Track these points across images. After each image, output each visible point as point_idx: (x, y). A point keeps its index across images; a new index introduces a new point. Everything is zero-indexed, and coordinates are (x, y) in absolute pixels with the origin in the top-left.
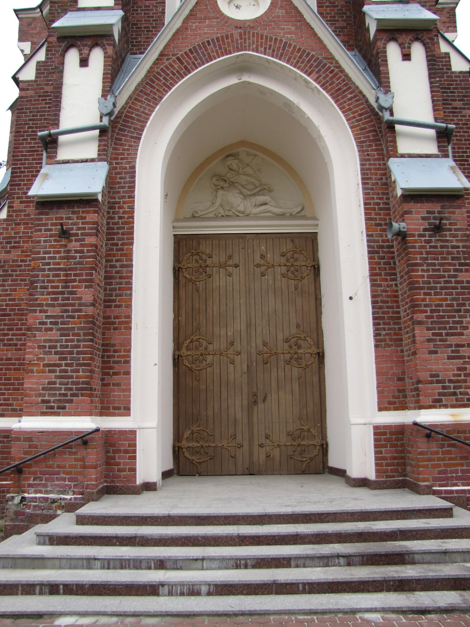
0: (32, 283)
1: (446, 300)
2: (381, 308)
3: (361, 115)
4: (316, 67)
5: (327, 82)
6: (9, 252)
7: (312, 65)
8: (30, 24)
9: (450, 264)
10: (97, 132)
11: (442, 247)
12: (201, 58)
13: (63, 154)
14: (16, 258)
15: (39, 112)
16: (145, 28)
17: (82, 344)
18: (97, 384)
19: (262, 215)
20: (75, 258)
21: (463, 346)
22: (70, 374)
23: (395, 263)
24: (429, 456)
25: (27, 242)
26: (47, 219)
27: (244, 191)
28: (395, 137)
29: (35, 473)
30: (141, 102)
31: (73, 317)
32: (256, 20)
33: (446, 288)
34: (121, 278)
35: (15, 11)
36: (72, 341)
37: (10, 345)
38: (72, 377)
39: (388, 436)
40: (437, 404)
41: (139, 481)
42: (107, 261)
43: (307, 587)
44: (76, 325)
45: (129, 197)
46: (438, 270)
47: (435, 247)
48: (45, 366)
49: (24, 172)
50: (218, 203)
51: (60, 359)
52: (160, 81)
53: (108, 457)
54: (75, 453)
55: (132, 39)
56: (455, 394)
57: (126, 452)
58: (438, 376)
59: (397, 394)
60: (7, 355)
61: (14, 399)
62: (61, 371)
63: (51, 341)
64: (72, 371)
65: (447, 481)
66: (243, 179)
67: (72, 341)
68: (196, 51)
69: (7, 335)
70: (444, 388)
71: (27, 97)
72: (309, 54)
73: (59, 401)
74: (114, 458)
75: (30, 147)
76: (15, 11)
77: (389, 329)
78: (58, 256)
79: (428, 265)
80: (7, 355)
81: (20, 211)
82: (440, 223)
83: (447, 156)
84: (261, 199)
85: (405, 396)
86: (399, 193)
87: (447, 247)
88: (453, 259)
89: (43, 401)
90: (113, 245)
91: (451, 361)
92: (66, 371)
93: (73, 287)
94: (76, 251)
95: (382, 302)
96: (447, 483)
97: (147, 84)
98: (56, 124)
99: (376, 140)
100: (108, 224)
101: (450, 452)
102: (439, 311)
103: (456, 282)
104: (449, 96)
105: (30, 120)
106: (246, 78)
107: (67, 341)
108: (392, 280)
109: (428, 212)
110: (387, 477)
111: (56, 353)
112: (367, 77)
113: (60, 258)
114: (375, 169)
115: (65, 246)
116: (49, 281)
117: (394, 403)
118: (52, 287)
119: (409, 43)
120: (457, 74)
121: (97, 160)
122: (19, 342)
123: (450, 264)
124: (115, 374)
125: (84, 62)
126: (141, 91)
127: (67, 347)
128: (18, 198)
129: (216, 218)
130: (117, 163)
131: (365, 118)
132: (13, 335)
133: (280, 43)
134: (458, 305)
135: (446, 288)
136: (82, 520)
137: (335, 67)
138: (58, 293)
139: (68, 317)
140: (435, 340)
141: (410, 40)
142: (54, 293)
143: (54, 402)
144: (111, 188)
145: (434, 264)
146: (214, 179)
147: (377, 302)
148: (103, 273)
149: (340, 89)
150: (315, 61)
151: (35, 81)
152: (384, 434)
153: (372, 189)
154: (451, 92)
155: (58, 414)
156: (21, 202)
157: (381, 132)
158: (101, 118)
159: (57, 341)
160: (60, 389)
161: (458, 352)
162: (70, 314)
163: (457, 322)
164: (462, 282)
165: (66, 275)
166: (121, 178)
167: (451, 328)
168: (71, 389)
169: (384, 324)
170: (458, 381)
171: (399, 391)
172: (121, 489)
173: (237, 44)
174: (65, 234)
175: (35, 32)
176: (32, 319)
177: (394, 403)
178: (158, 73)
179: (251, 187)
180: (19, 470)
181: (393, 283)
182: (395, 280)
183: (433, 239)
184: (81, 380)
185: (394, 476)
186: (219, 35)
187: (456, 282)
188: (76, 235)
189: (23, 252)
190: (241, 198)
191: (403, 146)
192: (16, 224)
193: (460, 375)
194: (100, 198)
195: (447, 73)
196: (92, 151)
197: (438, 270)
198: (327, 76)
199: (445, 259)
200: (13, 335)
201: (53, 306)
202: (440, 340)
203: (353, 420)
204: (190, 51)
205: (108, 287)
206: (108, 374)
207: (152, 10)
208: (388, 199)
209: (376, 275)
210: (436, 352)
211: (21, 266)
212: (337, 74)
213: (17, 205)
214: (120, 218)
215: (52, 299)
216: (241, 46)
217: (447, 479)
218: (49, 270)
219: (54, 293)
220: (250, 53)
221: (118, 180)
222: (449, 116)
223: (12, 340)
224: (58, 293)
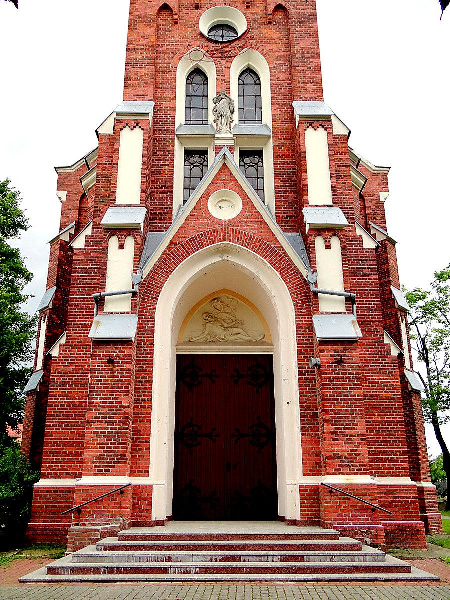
0: (91, 392)
1: (345, 407)
2: (306, 410)
3: (297, 285)
4: (270, 253)
5: (277, 263)
6: (68, 367)
7: (268, 251)
8: (66, 178)
9: (347, 385)
11: (343, 374)
12: (197, 246)
13: (108, 308)
14: (72, 371)
15: (87, 271)
16: (159, 213)
17: (121, 431)
18: (129, 456)
19: (236, 341)
20: (118, 377)
21: (355, 436)
22: (113, 450)
23: (315, 382)
24: (332, 505)
25: (80, 360)
26: (100, 352)
27: (224, 324)
28: (318, 301)
29: (89, 512)
30: (159, 274)
31: (116, 414)
32: (232, 221)
33: (345, 400)
34: (145, 389)
35: (55, 168)
36: (116, 429)
37: (67, 429)
38: (114, 452)
39: (309, 492)
40: (337, 472)
41: (153, 519)
42: (136, 378)
43: (248, 570)
44: (118, 419)
45: (151, 337)
46: (340, 389)
47: (339, 374)
48: (97, 444)
49: (78, 312)
50: (206, 333)
51: (107, 440)
52: (171, 260)
53: (134, 503)
54: (116, 499)
55: (151, 221)
56: (349, 466)
57: (146, 499)
58: (338, 454)
59: (315, 465)
60: (65, 436)
61: (68, 466)
62: (108, 448)
63: (102, 429)
64: (115, 448)
65: (343, 521)
66: (224, 316)
67: (116, 429)
68: (194, 241)
69: (65, 422)
70: (342, 462)
71: (80, 260)
72: (266, 243)
73: (107, 467)
74: (138, 503)
75: (82, 295)
76: (55, 168)
77: (311, 424)
78: (107, 375)
79: (334, 385)
80: (65, 436)
81: (75, 339)
82: (341, 358)
83: (353, 313)
84: (236, 330)
85: (320, 467)
86: (318, 339)
87: (346, 374)
88: (349, 381)
89: (96, 467)
90: (140, 367)
91: (347, 445)
92: (111, 448)
93: (117, 395)
94: (119, 373)
95: (307, 406)
96: (343, 523)
97: (162, 262)
98: (103, 286)
99: (307, 302)
100: (137, 354)
101: (345, 503)
102: (340, 414)
103: (351, 396)
104: (361, 266)
105: (81, 276)
106: (225, 258)
107: (112, 429)
108: (313, 393)
109: (335, 352)
110: (308, 518)
111: (105, 436)
113: (108, 377)
114: (305, 321)
115: (112, 370)
116: (101, 392)
117: (314, 471)
118: (103, 395)
119: (330, 238)
120: (367, 250)
121: (130, 313)
122: (73, 428)
123: (347, 385)
124: (140, 450)
125: (122, 247)
126: (158, 267)
127: (112, 433)
128: (74, 330)
129: (206, 343)
130: (143, 315)
131: (300, 288)
132: (69, 423)
133: (248, 236)
134: (352, 410)
135: (345, 400)
136: (122, 538)
137: (282, 253)
138: (106, 399)
139: (113, 414)
140: (337, 432)
141: (331, 236)
142: (104, 399)
143: (102, 468)
144: (139, 331)
145: (338, 385)
146: (205, 315)
147: (303, 407)
148: (134, 386)
149: (285, 268)
150: (269, 249)
151: (85, 249)
152: (307, 490)
153: (303, 334)
154: (363, 263)
155: (105, 475)
156: (76, 333)
157: (310, 296)
158: (133, 285)
159: (106, 429)
160: (107, 459)
161: (352, 440)
162: (114, 412)
163: (351, 421)
164: (355, 396)
165: (112, 388)
166: (145, 325)
167: (347, 425)
168: (114, 459)
169: (308, 420)
170: (351, 458)
171: (316, 463)
172: (142, 524)
173: (220, 236)
174: (111, 362)
175: (70, 184)
176: (90, 415)
177: (314, 471)
178: (169, 255)
179: (229, 321)
180: (79, 511)
181: (314, 394)
182: (316, 393)
183: (338, 369)
184: (120, 454)
185: (313, 519)
186: (209, 230)
188: (119, 363)
189: (77, 367)
190: (222, 330)
191: (323, 308)
192: (72, 348)
193: (352, 455)
194: (133, 339)
195: (361, 249)
196: (127, 307)
197: (340, 389)
198: (277, 259)
199: (345, 381)
200: (69, 423)
201: (104, 407)
202: (340, 432)
203: (288, 482)
204: (190, 240)
205: (137, 395)
206: (136, 450)
207: (164, 201)
208: (313, 341)
209: (302, 389)
210: (337, 440)
211: (76, 376)
212: (283, 257)
213: (73, 335)
214: (145, 350)
215: (103, 403)
216: (223, 238)
217: (344, 520)
218: (101, 384)
219: (104, 399)
220: (229, 243)
221: (144, 326)
222: (361, 279)
223: (68, 426)
224: (106, 399)
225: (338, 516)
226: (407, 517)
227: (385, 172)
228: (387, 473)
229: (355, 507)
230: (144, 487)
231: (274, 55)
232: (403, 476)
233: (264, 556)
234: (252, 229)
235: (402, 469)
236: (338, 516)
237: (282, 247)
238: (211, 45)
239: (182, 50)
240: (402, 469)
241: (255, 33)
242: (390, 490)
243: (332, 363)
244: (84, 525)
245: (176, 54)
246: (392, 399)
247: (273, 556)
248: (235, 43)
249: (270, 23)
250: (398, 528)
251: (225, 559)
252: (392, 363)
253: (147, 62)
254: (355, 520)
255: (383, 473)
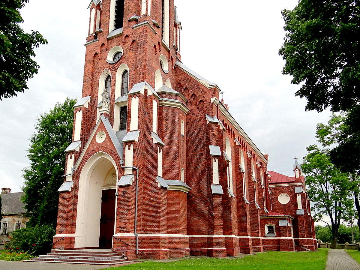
9: (126, 202)
10: (72, 175)
50: (113, 181)
57: (73, 241)
112: (221, 108)
123: (126, 202)
174: (64, 198)
187: (126, 206)
210: (121, 221)
225: (117, 247)
226: (155, 248)
227: (215, 87)
228: (152, 232)
229: (122, 244)
230: (73, 237)
231: (131, 64)
232: (157, 233)
233: (78, 257)
234: (108, 146)
235: (157, 230)
236: (117, 247)
237: (116, 151)
238: (111, 65)
239: (101, 70)
240: (157, 230)
241: (125, 55)
242: (151, 238)
243: (122, 194)
244: (55, 249)
245: (99, 73)
246: (157, 204)
247: (81, 257)
248: (118, 62)
249: (131, 49)
250: (152, 252)
251: (70, 258)
252: (158, 190)
253: (89, 80)
254: (122, 248)
255: (151, 232)
